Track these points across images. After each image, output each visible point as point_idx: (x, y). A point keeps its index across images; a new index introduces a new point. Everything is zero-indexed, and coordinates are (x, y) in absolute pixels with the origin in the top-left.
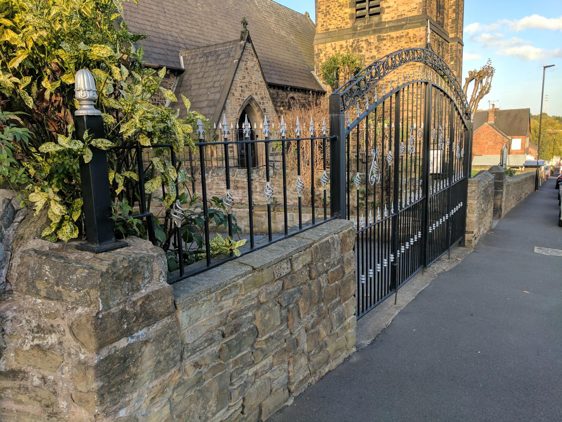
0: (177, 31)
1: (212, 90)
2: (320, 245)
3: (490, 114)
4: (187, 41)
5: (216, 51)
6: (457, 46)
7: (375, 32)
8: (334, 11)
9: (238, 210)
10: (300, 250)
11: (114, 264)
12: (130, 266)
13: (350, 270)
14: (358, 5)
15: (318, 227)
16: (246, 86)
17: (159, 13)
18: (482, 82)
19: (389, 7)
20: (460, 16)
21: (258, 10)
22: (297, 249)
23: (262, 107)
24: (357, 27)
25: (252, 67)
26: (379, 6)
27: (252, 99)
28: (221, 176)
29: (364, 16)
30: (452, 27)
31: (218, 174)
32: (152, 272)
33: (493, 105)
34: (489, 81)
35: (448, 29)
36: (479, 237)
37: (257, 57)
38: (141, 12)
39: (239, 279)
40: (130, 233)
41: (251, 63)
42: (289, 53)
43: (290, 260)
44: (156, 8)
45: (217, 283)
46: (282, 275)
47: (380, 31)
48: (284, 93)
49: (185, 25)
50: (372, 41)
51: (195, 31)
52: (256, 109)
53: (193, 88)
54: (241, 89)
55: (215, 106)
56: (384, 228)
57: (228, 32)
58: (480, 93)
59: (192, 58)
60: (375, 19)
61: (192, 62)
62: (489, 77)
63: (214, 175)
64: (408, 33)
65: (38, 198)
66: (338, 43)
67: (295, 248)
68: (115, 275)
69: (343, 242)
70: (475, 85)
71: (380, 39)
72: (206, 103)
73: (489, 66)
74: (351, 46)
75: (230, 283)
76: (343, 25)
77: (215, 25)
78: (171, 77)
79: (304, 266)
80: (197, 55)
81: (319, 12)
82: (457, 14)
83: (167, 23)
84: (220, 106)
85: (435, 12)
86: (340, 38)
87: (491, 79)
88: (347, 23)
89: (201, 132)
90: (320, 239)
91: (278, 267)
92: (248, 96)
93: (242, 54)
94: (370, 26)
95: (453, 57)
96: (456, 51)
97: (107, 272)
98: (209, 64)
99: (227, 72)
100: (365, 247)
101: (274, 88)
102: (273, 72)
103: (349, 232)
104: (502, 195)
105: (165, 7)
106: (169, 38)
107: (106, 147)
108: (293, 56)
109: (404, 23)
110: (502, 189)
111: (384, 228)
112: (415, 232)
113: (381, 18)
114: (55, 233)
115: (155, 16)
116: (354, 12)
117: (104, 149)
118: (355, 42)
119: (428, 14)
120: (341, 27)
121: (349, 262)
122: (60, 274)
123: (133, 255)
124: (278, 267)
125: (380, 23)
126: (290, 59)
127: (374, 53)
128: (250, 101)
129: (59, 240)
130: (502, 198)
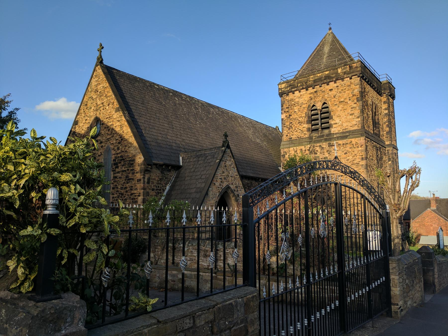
0: (180, 140)
1: (200, 181)
2: (223, 306)
3: (432, 202)
4: (187, 147)
5: (205, 154)
6: (393, 150)
7: (326, 140)
8: (296, 126)
9: (204, 274)
10: (203, 309)
11: (43, 311)
12: (56, 312)
13: (253, 329)
14: (313, 122)
15: (228, 292)
16: (225, 178)
17: (168, 128)
18: (412, 178)
19: (336, 124)
20: (393, 129)
21: (241, 126)
22: (201, 309)
23: (236, 193)
24: (313, 137)
25: (230, 165)
26: (328, 123)
27: (228, 187)
28: (195, 246)
29: (318, 130)
30: (387, 137)
31: (193, 245)
32: (73, 318)
33: (434, 194)
34: (418, 178)
35: (384, 138)
36: (407, 310)
37: (234, 159)
38: (156, 128)
39: (144, 329)
40: (66, 290)
41: (230, 162)
42: (262, 154)
43: (193, 317)
44: (168, 126)
45: (125, 331)
46: (184, 329)
47: (330, 139)
48: (257, 183)
49: (186, 136)
50: (324, 146)
51: (193, 140)
52: (231, 195)
53: (187, 179)
54: (220, 180)
55: (201, 192)
56: (321, 295)
57: (217, 141)
58: (411, 186)
59: (188, 158)
60: (326, 131)
61: (188, 161)
62: (417, 174)
63: (190, 245)
64: (351, 142)
65: (11, 264)
66: (299, 148)
67: (199, 308)
68: (43, 319)
69: (246, 305)
70: (406, 180)
71: (331, 145)
72: (195, 189)
73: (415, 166)
74: (309, 150)
75: (136, 331)
76: (302, 135)
77: (208, 136)
78: (172, 171)
79: (207, 323)
80: (192, 156)
81: (285, 127)
82: (390, 128)
83: (174, 135)
84: (204, 193)
85: (371, 127)
86: (300, 144)
87: (419, 176)
88: (305, 134)
89: (131, 223)
90: (223, 302)
91: (180, 322)
92: (225, 185)
93: (223, 156)
94: (323, 136)
95: (390, 159)
96: (392, 154)
97: (37, 315)
98: (199, 163)
99: (211, 168)
100: (280, 310)
101: (249, 180)
102: (249, 168)
103: (253, 297)
104: (434, 272)
105: (174, 124)
106: (174, 144)
107: (55, 234)
108: (265, 157)
109: (348, 134)
110: (433, 266)
111: (321, 295)
112: (331, 300)
113: (330, 131)
114: (19, 287)
115: (166, 130)
116: (310, 127)
117: (54, 234)
118: (312, 147)
119: (366, 128)
120: (301, 137)
121: (252, 323)
122: (10, 316)
123: (60, 305)
124: (180, 322)
125: (330, 134)
126: (263, 158)
127: (327, 155)
128: (227, 189)
129: (20, 292)
130: (434, 275)
